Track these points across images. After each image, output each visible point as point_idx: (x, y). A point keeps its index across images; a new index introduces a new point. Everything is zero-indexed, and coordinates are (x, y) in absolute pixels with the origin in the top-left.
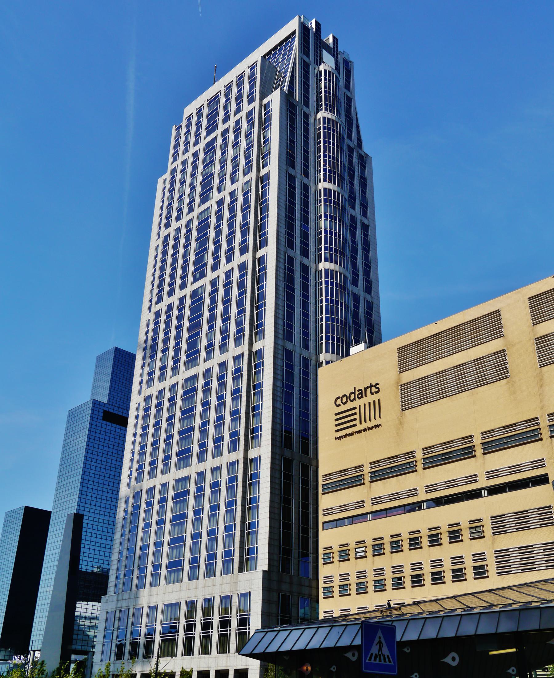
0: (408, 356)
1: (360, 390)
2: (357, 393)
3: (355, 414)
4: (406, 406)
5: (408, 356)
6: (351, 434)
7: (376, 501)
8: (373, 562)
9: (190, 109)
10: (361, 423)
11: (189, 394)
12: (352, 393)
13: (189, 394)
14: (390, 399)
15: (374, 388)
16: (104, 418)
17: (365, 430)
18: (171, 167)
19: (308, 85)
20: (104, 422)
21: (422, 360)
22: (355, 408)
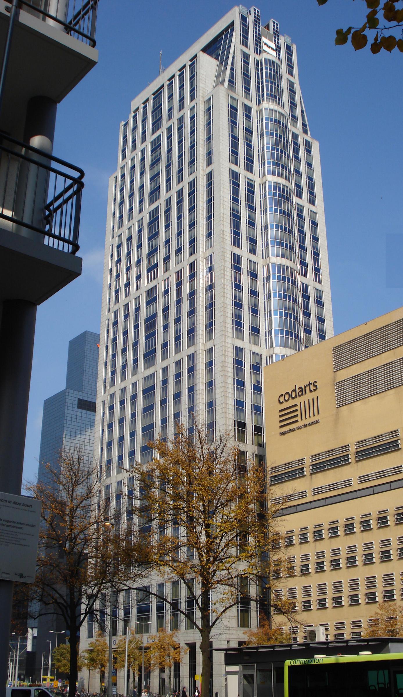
0: (343, 355)
1: (301, 388)
2: (298, 391)
3: (296, 410)
4: (342, 403)
5: (343, 355)
6: (294, 430)
7: (317, 491)
8: (315, 546)
9: (137, 102)
10: (302, 419)
11: (149, 391)
12: (293, 391)
13: (149, 391)
14: (326, 396)
15: (313, 386)
16: (79, 407)
17: (306, 426)
18: (120, 163)
19: (248, 76)
20: (80, 410)
21: (354, 360)
22: (296, 405)
